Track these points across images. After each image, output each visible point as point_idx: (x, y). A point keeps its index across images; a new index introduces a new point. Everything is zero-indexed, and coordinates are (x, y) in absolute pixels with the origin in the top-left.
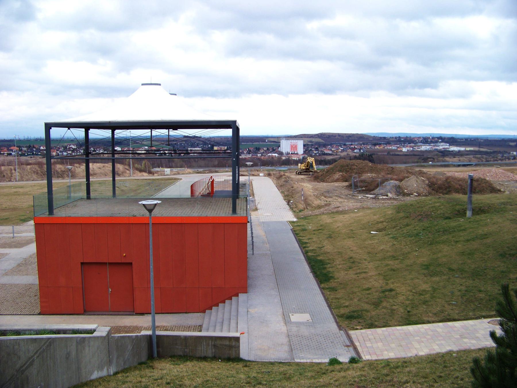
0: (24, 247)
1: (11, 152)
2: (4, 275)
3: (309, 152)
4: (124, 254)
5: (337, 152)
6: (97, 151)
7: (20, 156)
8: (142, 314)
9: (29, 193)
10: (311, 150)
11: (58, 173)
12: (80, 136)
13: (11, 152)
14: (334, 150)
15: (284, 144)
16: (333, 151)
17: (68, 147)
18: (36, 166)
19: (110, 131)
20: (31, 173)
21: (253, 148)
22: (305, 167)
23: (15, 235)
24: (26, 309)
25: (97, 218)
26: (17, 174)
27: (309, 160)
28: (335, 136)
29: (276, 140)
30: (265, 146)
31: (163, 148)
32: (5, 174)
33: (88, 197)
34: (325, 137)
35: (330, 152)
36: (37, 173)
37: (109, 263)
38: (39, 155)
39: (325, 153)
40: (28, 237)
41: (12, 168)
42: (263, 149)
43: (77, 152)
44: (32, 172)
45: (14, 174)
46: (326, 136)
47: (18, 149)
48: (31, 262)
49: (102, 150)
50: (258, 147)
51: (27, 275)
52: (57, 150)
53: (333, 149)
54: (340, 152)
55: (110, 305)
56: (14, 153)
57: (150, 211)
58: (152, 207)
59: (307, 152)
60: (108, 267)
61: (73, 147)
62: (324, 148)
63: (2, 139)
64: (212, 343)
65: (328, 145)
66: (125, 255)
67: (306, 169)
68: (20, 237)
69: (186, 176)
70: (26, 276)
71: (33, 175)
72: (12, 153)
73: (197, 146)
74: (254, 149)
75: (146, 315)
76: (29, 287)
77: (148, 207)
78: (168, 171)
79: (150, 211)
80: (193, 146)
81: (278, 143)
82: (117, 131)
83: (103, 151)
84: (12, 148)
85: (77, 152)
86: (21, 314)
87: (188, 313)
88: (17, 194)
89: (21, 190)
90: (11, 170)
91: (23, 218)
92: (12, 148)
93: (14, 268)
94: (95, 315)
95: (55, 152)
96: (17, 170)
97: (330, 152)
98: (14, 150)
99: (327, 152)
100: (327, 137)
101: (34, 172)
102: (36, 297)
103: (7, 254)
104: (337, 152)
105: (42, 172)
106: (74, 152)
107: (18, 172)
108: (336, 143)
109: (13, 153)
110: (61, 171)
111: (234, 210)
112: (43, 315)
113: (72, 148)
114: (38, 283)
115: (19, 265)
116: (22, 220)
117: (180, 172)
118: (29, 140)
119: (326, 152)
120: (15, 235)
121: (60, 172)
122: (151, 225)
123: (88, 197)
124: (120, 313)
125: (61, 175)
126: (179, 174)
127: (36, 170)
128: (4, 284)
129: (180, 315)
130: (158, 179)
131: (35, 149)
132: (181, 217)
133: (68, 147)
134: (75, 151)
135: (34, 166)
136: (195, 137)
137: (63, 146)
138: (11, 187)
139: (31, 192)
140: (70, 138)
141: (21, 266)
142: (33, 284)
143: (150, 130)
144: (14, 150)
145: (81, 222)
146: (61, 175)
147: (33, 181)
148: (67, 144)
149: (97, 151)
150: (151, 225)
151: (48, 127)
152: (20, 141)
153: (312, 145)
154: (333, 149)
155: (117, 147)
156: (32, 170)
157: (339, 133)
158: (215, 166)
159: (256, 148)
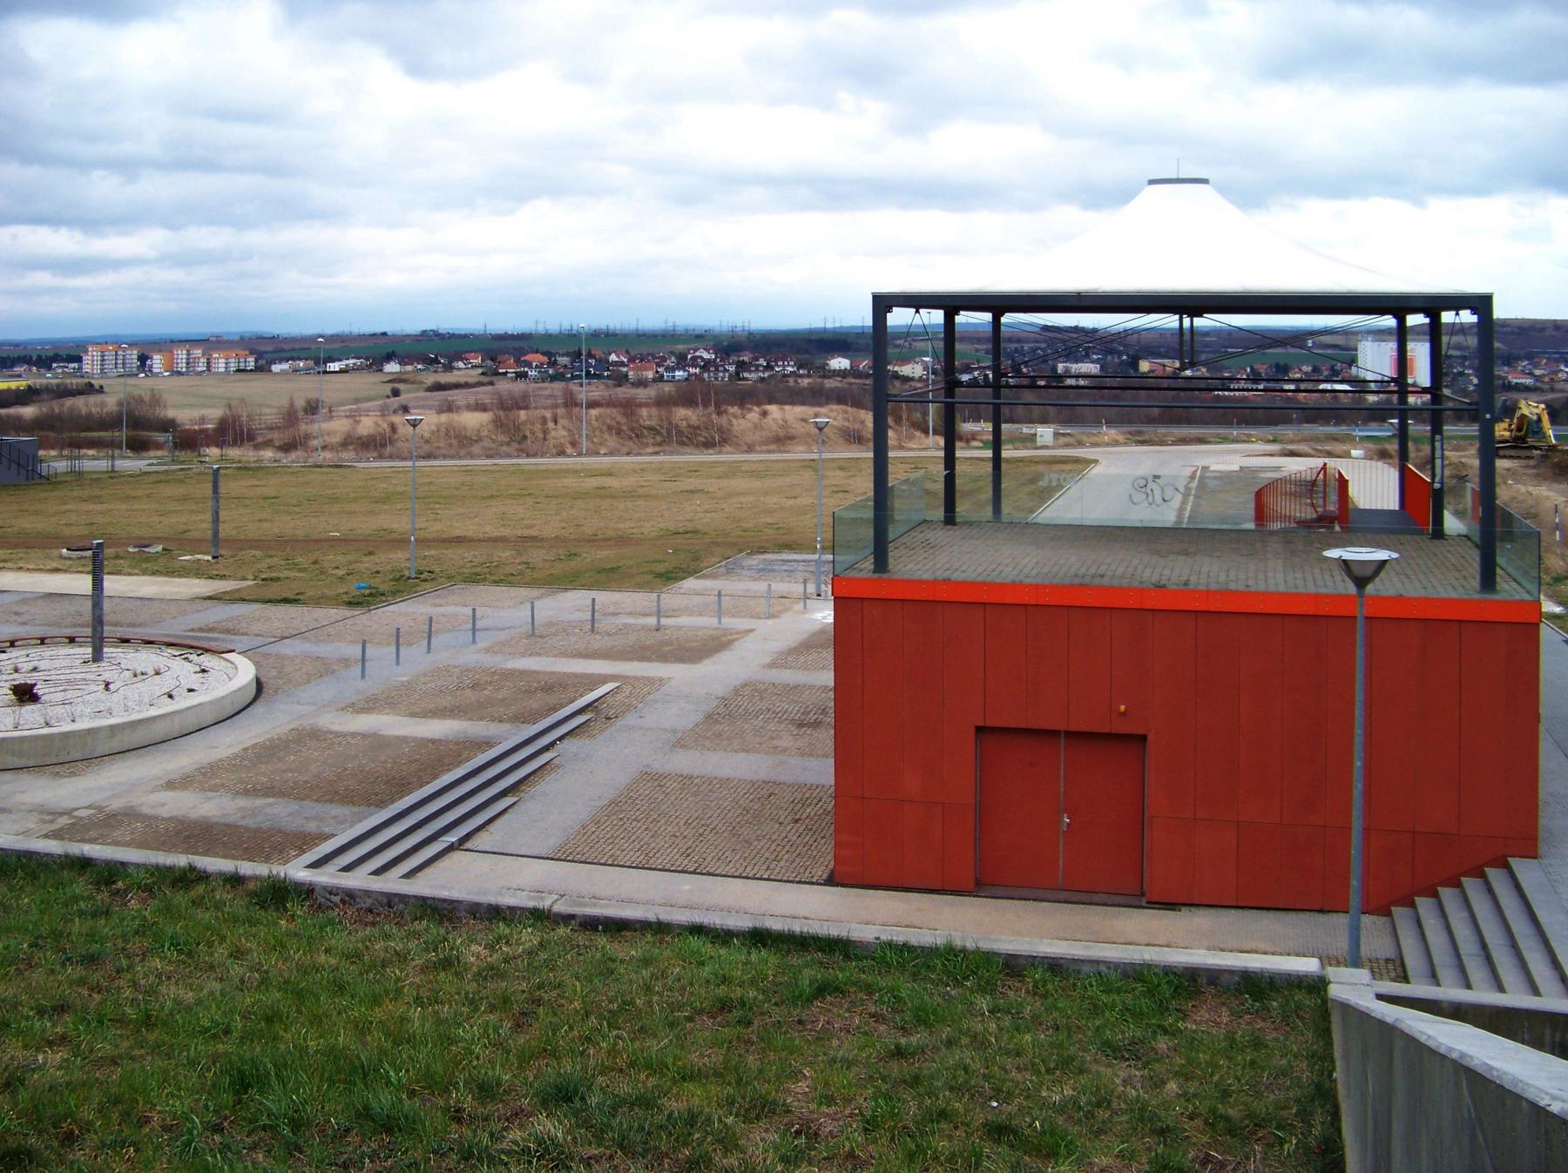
0: (705, 662)
1: (526, 369)
2: (674, 746)
3: (1453, 379)
4: (1123, 708)
5: (1552, 379)
6: (777, 369)
7: (551, 381)
8: (1171, 906)
9: (641, 491)
10: (1461, 374)
11: (680, 432)
12: (724, 324)
13: (526, 369)
14: (1543, 376)
15: (1369, 352)
16: (1538, 378)
17: (689, 356)
18: (614, 410)
19: (987, 317)
20: (601, 432)
21: (1265, 367)
22: (1511, 431)
23: (664, 621)
24: (782, 863)
25: (1036, 588)
26: (559, 433)
27: (1525, 411)
28: (1543, 329)
29: (1339, 340)
30: (1305, 361)
31: (978, 362)
32: (528, 433)
33: (950, 519)
34: (1505, 333)
35: (1528, 381)
36: (619, 432)
37: (1065, 732)
38: (604, 378)
39: (1509, 382)
40: (699, 628)
41: (548, 415)
42: (1300, 370)
43: (717, 370)
44: (605, 428)
45: (553, 434)
46: (1509, 330)
47: (546, 359)
48: (746, 710)
49: (793, 366)
50: (1282, 363)
51: (747, 751)
52: (658, 365)
53: (1537, 372)
54: (1564, 380)
55: (1061, 864)
56: (534, 373)
57: (1361, 582)
58: (1369, 571)
59: (1449, 379)
60: (1062, 745)
61: (706, 356)
62: (1506, 368)
63: (501, 332)
64: (1553, 1036)
65: (1519, 358)
66: (1126, 710)
67: (1516, 439)
68: (679, 628)
69: (1110, 453)
70: (743, 755)
71: (607, 436)
72: (530, 373)
73: (1086, 357)
74: (1270, 367)
75: (1183, 909)
76: (803, 794)
77: (1357, 571)
78: (1045, 433)
79: (1361, 582)
80: (1072, 355)
81: (1347, 349)
82: (1008, 318)
83: (795, 369)
84: (528, 357)
85: (717, 370)
86: (772, 877)
87: (1329, 911)
88: (602, 493)
89: (613, 483)
90: (544, 420)
91: (660, 568)
92: (528, 357)
93: (697, 725)
94: (1013, 899)
95: (652, 369)
96: (561, 421)
97: (1528, 381)
98: (534, 364)
99: (1519, 381)
100: (1512, 333)
101: (610, 428)
102: (798, 825)
103: (661, 681)
104: (1552, 379)
105: (632, 430)
106: (709, 371)
107: (564, 427)
108: (1548, 353)
109: (532, 373)
110: (689, 426)
111: (1488, 579)
112: (843, 885)
113: (701, 357)
114: (832, 782)
115: (710, 718)
116: (659, 575)
117: (1085, 438)
118: (575, 335)
119: (1515, 381)
120: (664, 621)
121: (685, 430)
122: (1360, 625)
123: (950, 519)
124: (1096, 898)
125: (688, 437)
126: (1080, 444)
127: (614, 423)
128: (684, 774)
129: (1302, 916)
130: (1021, 460)
131: (592, 361)
132: (1317, 596)
133: (689, 356)
134: (711, 369)
135: (608, 411)
136: (1076, 329)
137: (672, 353)
138: (576, 472)
139: (645, 489)
140: (694, 330)
141: (717, 722)
142: (774, 783)
143: (1177, 317)
144: (534, 364)
145: (985, 598)
146: (688, 437)
147: (628, 454)
148: (686, 346)
149: (777, 369)
150: (1360, 625)
151: (883, 304)
152: (548, 337)
153: (1464, 358)
154: (1537, 372)
155: (839, 356)
156: (604, 423)
157: (1555, 320)
158: (1151, 421)
159: (1277, 366)
